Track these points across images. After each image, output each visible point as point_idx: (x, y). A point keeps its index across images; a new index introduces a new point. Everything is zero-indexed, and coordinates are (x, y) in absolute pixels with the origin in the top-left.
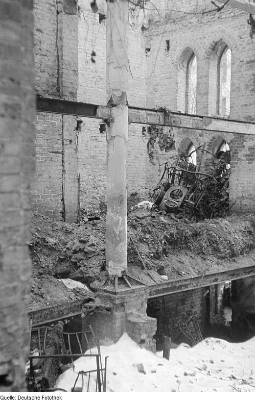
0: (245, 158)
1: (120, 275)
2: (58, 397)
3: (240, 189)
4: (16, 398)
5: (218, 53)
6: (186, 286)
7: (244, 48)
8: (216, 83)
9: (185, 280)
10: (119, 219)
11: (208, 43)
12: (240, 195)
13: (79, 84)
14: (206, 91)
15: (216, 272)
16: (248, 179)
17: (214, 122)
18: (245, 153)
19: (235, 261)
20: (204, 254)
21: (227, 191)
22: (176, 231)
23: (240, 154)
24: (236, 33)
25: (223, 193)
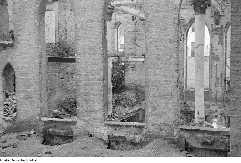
0: (131, 69)
1: (111, 115)
2: (36, 160)
3: (129, 80)
4: (10, 161)
5: (117, 26)
6: (123, 118)
7: (129, 26)
8: (117, 38)
9: (123, 116)
10: (110, 96)
11: (114, 22)
12: (129, 83)
13: (37, 28)
14: (114, 41)
15: (129, 112)
16: (132, 77)
17: (130, 58)
18: (131, 67)
19: (133, 108)
20: (125, 106)
21: (124, 81)
22: (117, 98)
23: (129, 67)
24: (126, 20)
25: (122, 82)
